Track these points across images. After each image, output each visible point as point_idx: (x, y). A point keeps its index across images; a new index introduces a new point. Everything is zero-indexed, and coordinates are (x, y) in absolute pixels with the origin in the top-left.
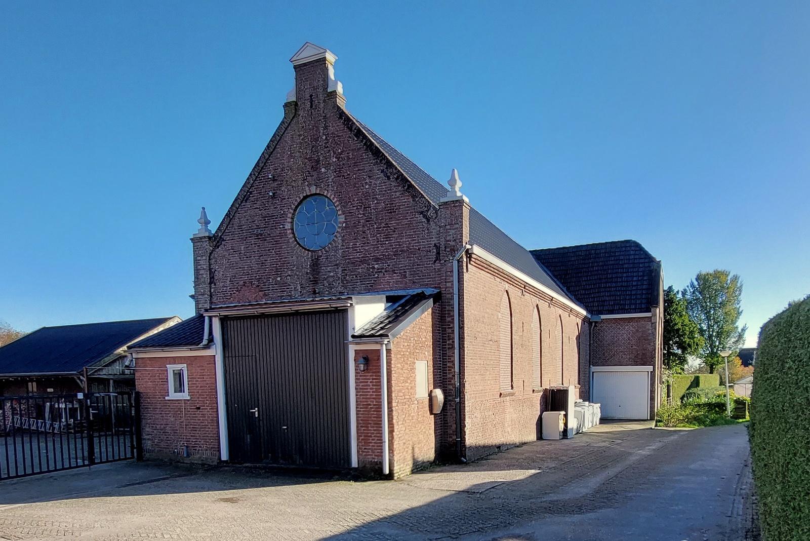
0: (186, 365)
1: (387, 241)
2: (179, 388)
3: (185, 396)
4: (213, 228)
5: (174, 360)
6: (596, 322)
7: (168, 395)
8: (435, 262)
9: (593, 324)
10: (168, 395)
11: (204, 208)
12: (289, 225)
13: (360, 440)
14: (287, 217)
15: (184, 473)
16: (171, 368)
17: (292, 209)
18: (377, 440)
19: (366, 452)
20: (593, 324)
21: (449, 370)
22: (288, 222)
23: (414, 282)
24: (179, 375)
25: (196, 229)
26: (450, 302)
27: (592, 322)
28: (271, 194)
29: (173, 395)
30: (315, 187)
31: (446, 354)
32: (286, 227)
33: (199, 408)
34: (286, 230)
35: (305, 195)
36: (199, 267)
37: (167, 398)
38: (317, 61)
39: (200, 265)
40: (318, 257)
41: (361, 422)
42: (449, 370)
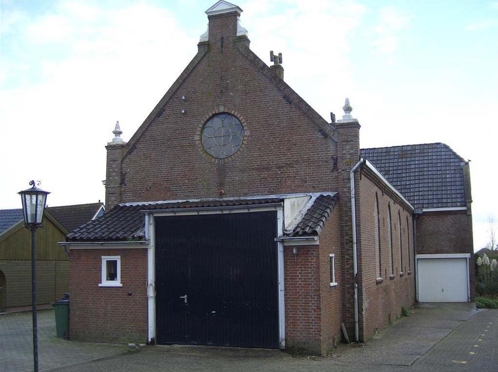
0: (119, 257)
1: (288, 152)
2: (112, 276)
3: (117, 283)
4: (126, 138)
5: (109, 252)
6: (418, 214)
7: (101, 283)
8: (333, 171)
9: (416, 216)
10: (101, 283)
11: (118, 122)
12: (198, 137)
13: (289, 323)
14: (196, 130)
15: (296, 338)
16: (105, 259)
17: (201, 123)
18: (305, 323)
19: (295, 334)
20: (416, 216)
21: (346, 262)
22: (198, 135)
23: (313, 187)
24: (112, 265)
25: (110, 138)
26: (346, 204)
27: (415, 214)
28: (183, 112)
29: (105, 283)
30: (223, 107)
31: (344, 247)
32: (196, 139)
33: (130, 295)
34: (195, 140)
35: (214, 113)
36: (111, 170)
37: (100, 285)
38: (231, 13)
39: (113, 168)
40: (224, 164)
41: (290, 307)
42: (346, 262)
